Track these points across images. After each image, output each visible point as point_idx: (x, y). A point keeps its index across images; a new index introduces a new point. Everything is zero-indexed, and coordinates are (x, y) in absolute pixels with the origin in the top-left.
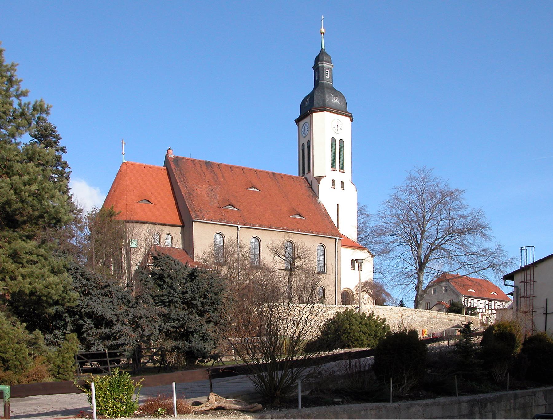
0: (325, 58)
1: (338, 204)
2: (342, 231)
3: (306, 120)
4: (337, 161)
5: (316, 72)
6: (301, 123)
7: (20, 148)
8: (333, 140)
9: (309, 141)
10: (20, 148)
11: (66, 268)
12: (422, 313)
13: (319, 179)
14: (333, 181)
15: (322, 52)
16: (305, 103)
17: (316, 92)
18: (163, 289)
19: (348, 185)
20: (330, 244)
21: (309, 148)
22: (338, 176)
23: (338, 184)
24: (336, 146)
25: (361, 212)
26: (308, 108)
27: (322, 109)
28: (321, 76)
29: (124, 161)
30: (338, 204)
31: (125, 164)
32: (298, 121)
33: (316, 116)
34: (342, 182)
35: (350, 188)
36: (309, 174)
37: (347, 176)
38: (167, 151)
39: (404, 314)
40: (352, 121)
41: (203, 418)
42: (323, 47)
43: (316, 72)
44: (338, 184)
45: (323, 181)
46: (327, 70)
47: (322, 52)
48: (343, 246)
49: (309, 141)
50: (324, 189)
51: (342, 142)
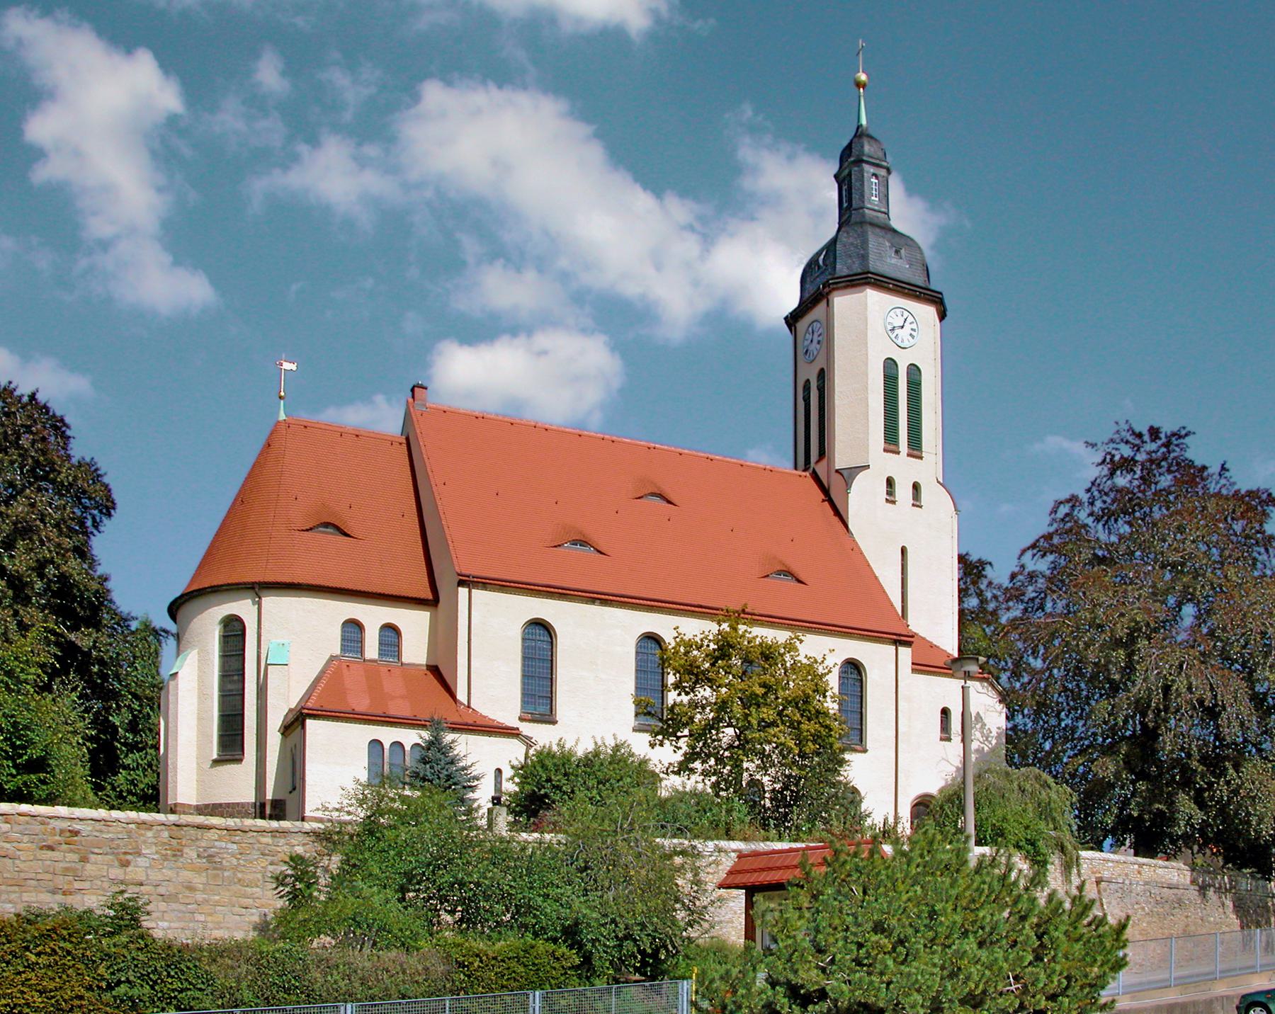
0: (867, 148)
1: (904, 551)
3: (818, 312)
4: (902, 430)
6: (802, 325)
7: (674, 782)
8: (890, 365)
9: (822, 375)
10: (675, 781)
11: (696, 875)
12: (1160, 871)
13: (848, 475)
14: (890, 482)
15: (860, 134)
17: (843, 238)
19: (935, 496)
20: (878, 659)
21: (821, 390)
22: (903, 468)
23: (904, 492)
24: (900, 387)
25: (971, 570)
27: (865, 279)
28: (855, 196)
29: (282, 417)
30: (904, 551)
31: (283, 427)
33: (842, 303)
34: (916, 487)
35: (938, 500)
36: (824, 462)
37: (929, 469)
38: (413, 390)
39: (1106, 874)
40: (942, 316)
42: (864, 122)
43: (845, 188)
44: (904, 492)
46: (874, 180)
47: (860, 134)
48: (919, 667)
49: (822, 375)
50: (863, 500)
51: (914, 371)
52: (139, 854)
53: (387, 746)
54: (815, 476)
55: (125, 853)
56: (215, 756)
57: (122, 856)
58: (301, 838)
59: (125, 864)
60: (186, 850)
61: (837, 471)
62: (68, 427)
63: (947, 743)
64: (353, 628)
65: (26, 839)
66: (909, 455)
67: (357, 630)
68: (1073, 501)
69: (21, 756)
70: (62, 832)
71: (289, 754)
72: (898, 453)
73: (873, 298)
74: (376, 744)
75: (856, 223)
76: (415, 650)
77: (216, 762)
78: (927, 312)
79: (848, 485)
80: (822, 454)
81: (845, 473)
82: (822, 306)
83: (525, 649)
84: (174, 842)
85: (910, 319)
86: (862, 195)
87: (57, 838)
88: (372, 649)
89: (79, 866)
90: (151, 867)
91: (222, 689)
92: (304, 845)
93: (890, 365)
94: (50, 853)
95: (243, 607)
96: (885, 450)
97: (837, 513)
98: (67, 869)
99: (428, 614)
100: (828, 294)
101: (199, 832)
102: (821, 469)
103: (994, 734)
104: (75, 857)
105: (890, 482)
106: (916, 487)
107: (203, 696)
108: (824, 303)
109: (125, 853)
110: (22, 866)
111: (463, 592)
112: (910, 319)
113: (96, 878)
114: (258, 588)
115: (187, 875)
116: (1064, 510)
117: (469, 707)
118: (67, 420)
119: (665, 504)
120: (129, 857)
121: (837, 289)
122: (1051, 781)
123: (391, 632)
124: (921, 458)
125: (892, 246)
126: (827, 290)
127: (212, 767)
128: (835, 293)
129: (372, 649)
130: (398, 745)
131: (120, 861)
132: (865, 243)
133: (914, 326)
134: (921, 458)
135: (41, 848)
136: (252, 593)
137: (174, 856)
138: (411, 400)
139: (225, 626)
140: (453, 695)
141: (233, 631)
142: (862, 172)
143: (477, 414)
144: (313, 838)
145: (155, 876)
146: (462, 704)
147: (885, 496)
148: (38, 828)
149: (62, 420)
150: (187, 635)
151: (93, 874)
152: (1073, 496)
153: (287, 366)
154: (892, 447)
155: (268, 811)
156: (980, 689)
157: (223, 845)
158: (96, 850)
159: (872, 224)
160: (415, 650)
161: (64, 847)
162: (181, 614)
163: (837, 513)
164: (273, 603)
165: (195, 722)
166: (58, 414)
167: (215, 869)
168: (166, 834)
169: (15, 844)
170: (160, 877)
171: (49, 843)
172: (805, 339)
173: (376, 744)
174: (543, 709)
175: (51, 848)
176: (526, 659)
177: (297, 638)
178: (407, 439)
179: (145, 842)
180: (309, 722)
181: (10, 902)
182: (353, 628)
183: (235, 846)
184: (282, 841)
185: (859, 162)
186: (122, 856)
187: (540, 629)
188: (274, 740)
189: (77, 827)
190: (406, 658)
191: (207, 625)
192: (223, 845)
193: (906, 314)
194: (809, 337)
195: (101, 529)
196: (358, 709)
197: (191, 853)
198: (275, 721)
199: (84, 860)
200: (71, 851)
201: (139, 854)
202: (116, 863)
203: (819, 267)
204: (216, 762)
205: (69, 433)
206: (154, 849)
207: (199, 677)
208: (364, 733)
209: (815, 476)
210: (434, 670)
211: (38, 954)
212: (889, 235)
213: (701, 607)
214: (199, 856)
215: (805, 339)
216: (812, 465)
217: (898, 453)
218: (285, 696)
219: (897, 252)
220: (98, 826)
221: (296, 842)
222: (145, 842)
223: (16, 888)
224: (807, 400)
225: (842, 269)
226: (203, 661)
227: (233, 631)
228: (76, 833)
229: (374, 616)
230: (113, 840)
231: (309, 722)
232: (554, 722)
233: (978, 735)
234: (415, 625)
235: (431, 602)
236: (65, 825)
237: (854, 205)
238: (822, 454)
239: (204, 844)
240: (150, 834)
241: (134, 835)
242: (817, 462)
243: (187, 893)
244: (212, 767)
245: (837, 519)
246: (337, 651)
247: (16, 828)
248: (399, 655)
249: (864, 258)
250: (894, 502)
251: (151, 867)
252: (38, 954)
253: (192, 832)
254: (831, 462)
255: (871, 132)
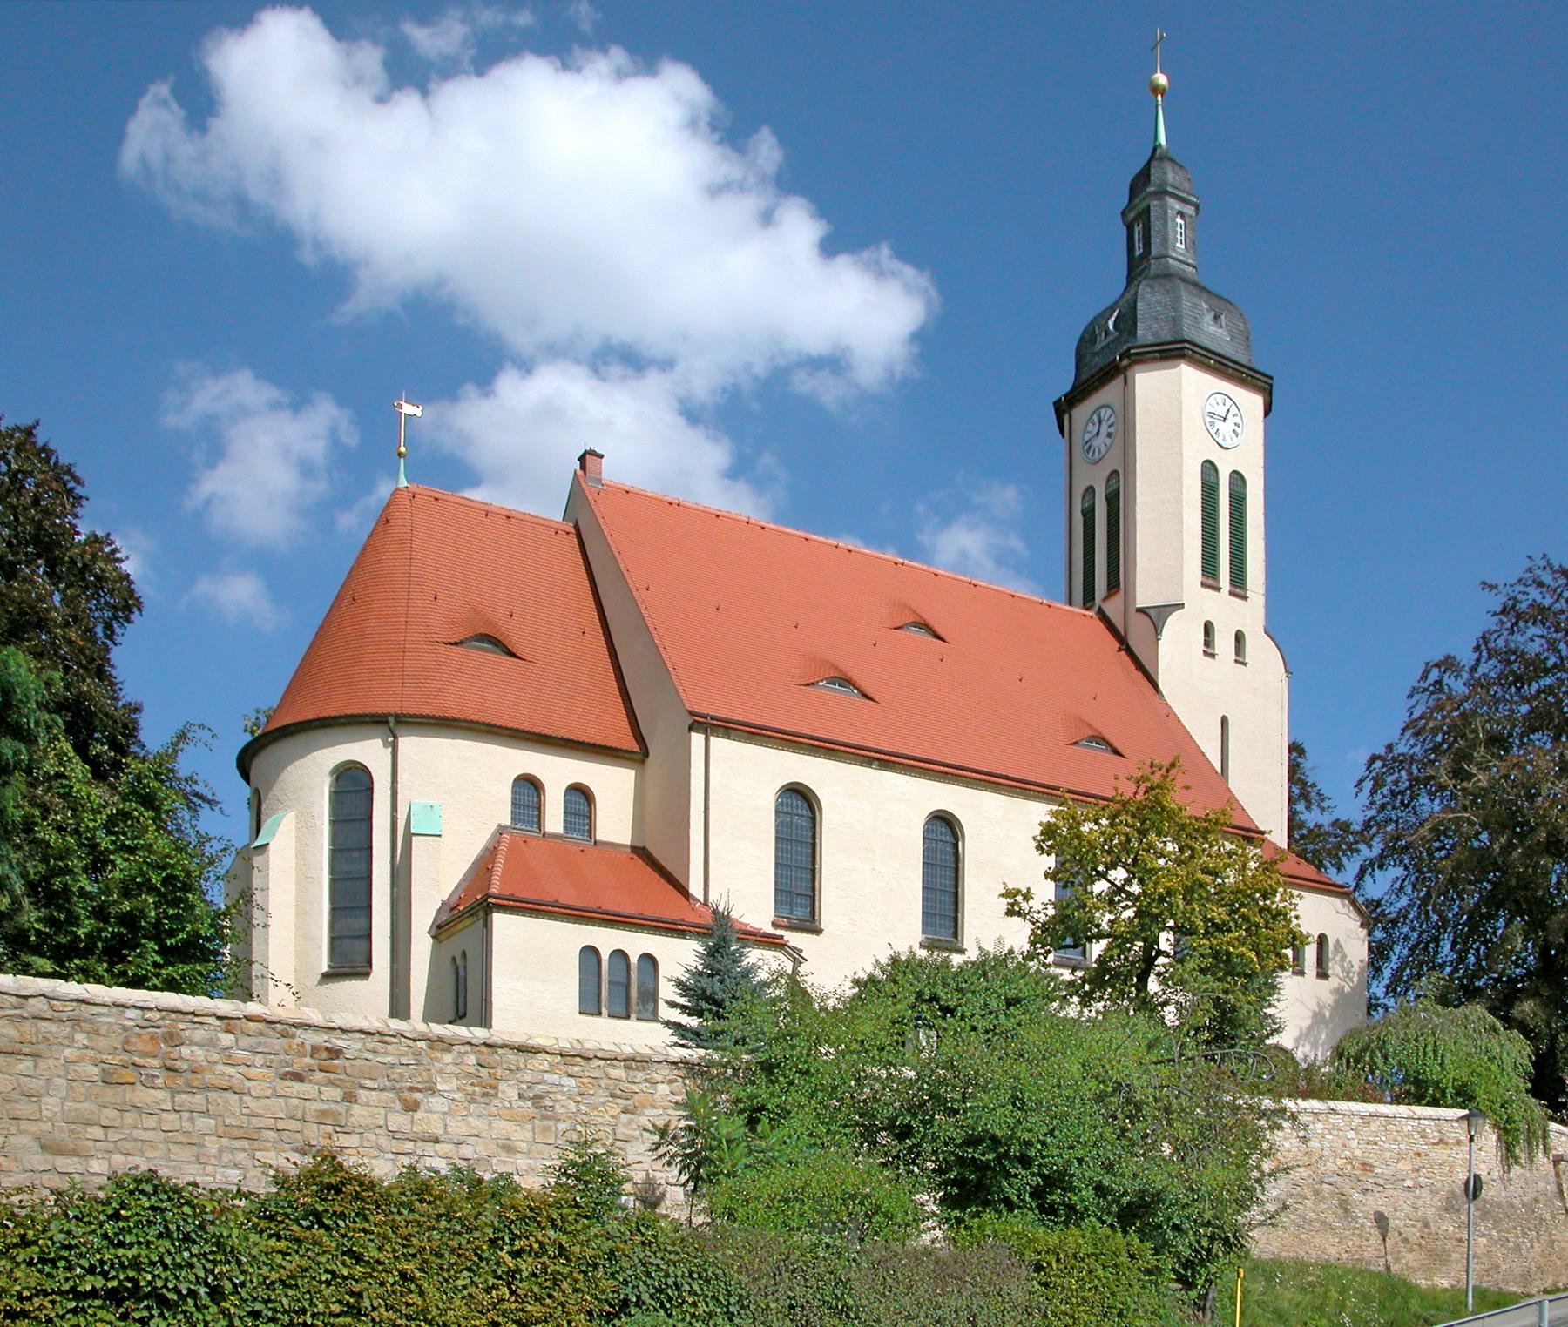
0: (1170, 176)
1: (1224, 721)
2: (691, 891)
3: (1109, 393)
4: (1220, 563)
5: (1138, 229)
6: (1081, 412)
8: (1209, 468)
13: (1156, 617)
14: (1208, 628)
16: (1093, 340)
18: (773, 1083)
19: (1262, 650)
21: (1113, 499)
22: (1220, 607)
23: (1224, 643)
26: (1104, 362)
27: (1173, 351)
28: (1155, 241)
30: (1224, 721)
32: (1064, 408)
33: (1148, 383)
34: (1239, 638)
36: (1118, 600)
37: (1250, 614)
38: (582, 459)
41: (265, 889)
42: (1162, 140)
43: (1138, 229)
44: (1224, 643)
45: (1172, 624)
46: (1179, 220)
47: (1155, 155)
50: (1175, 654)
51: (1237, 479)
52: (432, 1090)
53: (605, 956)
54: (1103, 617)
55: (412, 1089)
56: (325, 969)
57: (407, 1095)
58: (665, 1071)
59: (411, 1107)
60: (502, 1086)
61: (1140, 610)
62: (78, 481)
63: (1299, 978)
64: (529, 786)
65: (259, 1060)
66: (1231, 593)
67: (532, 791)
68: (1448, 664)
69: (172, 933)
70: (315, 1049)
71: (448, 969)
72: (1218, 589)
73: (1190, 380)
74: (590, 952)
75: (1157, 277)
76: (615, 822)
77: (327, 977)
78: (1252, 402)
79: (1157, 629)
80: (1113, 584)
81: (1152, 613)
82: (1115, 386)
83: (779, 827)
84: (484, 1072)
85: (1234, 410)
86: (1165, 240)
87: (308, 1060)
88: (554, 821)
89: (341, 1108)
90: (450, 1112)
91: (332, 871)
92: (671, 1082)
93: (1209, 468)
94: (297, 1086)
95: (369, 751)
96: (1203, 585)
97: (1139, 666)
98: (323, 1113)
99: (633, 772)
100: (1126, 368)
101: (521, 1057)
102: (1113, 609)
103: (1356, 968)
104: (336, 1093)
105: (1208, 628)
106: (1239, 638)
107: (304, 879)
108: (1119, 380)
109: (412, 1089)
110: (253, 1105)
111: (697, 739)
112: (1234, 410)
113: (368, 1128)
114: (389, 724)
115: (504, 1127)
116: (1434, 675)
117: (706, 904)
118: (78, 472)
119: (931, 639)
120: (418, 1096)
121: (1141, 362)
122: (1498, 1024)
123: (580, 795)
124: (1245, 598)
125: (1211, 309)
126: (1125, 362)
127: (320, 983)
128: (1137, 367)
129: (554, 821)
130: (619, 955)
131: (404, 1101)
132: (1177, 300)
133: (1238, 419)
134: (1245, 598)
135: (283, 1077)
136: (383, 729)
137: (485, 1095)
138: (580, 473)
139: (338, 779)
140: (683, 891)
141: (352, 787)
142: (1164, 208)
143: (669, 499)
144: (682, 1073)
145: (457, 1127)
146: (697, 900)
147: (1202, 647)
148: (278, 1043)
149: (69, 472)
150: (276, 790)
151: (363, 1122)
152: (1448, 657)
153: (408, 409)
154: (1210, 582)
155: (1310, 952)
156: (1341, 909)
157: (555, 1079)
158: (369, 1083)
159: (1183, 280)
160: (615, 822)
161: (319, 1076)
162: (257, 766)
163: (1139, 666)
164: (409, 744)
165: (292, 917)
166: (63, 461)
167: (545, 1117)
168: (472, 1059)
169: (242, 1069)
170: (464, 1130)
171: (296, 1068)
172: (1085, 431)
173: (590, 952)
174: (800, 912)
175: (299, 1077)
176: (781, 839)
177: (451, 797)
178: (576, 527)
179: (441, 1071)
180: (498, 918)
181: (236, 1166)
182: (529, 786)
183: (572, 1082)
184: (640, 1076)
185: (1162, 193)
186: (407, 1095)
187: (799, 803)
188: (422, 947)
189: (338, 1042)
190: (602, 834)
191: (310, 776)
192: (555, 1079)
193: (1229, 402)
194: (1093, 429)
195: (118, 639)
196: (563, 900)
197: (509, 1091)
198: (423, 917)
199: (350, 1098)
200: (331, 1083)
201: (432, 1090)
202: (398, 1106)
203: (1107, 333)
204: (327, 977)
205: (79, 490)
206: (454, 1083)
207: (299, 853)
208: (574, 936)
209: (1103, 617)
210: (640, 852)
211: (516, 1254)
212: (1204, 295)
213: (1007, 778)
214: (520, 1096)
215: (1085, 431)
216: (1098, 601)
217: (1218, 589)
218: (438, 880)
219: (1216, 318)
220: (371, 1042)
221: (659, 1078)
222: (441, 1071)
223: (245, 1144)
224: (1088, 515)
225: (1144, 333)
226: (305, 829)
227: (352, 787)
228: (336, 1053)
229: (558, 772)
230: (393, 1066)
231: (498, 918)
232: (818, 931)
233: (1338, 969)
234: (614, 788)
235: (634, 753)
236: (319, 1039)
237: (1154, 252)
238: (1113, 584)
239: (528, 1077)
240: (448, 1058)
241: (426, 1060)
242: (1105, 599)
243: (504, 1156)
244: (320, 983)
245: (1140, 675)
246: (508, 822)
247: (244, 1042)
248: (591, 831)
249: (1176, 321)
250: (1213, 656)
251: (450, 1112)
252: (516, 1254)
253: (511, 1057)
254: (1129, 597)
255: (1172, 154)
